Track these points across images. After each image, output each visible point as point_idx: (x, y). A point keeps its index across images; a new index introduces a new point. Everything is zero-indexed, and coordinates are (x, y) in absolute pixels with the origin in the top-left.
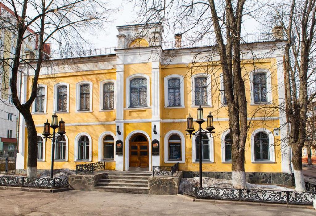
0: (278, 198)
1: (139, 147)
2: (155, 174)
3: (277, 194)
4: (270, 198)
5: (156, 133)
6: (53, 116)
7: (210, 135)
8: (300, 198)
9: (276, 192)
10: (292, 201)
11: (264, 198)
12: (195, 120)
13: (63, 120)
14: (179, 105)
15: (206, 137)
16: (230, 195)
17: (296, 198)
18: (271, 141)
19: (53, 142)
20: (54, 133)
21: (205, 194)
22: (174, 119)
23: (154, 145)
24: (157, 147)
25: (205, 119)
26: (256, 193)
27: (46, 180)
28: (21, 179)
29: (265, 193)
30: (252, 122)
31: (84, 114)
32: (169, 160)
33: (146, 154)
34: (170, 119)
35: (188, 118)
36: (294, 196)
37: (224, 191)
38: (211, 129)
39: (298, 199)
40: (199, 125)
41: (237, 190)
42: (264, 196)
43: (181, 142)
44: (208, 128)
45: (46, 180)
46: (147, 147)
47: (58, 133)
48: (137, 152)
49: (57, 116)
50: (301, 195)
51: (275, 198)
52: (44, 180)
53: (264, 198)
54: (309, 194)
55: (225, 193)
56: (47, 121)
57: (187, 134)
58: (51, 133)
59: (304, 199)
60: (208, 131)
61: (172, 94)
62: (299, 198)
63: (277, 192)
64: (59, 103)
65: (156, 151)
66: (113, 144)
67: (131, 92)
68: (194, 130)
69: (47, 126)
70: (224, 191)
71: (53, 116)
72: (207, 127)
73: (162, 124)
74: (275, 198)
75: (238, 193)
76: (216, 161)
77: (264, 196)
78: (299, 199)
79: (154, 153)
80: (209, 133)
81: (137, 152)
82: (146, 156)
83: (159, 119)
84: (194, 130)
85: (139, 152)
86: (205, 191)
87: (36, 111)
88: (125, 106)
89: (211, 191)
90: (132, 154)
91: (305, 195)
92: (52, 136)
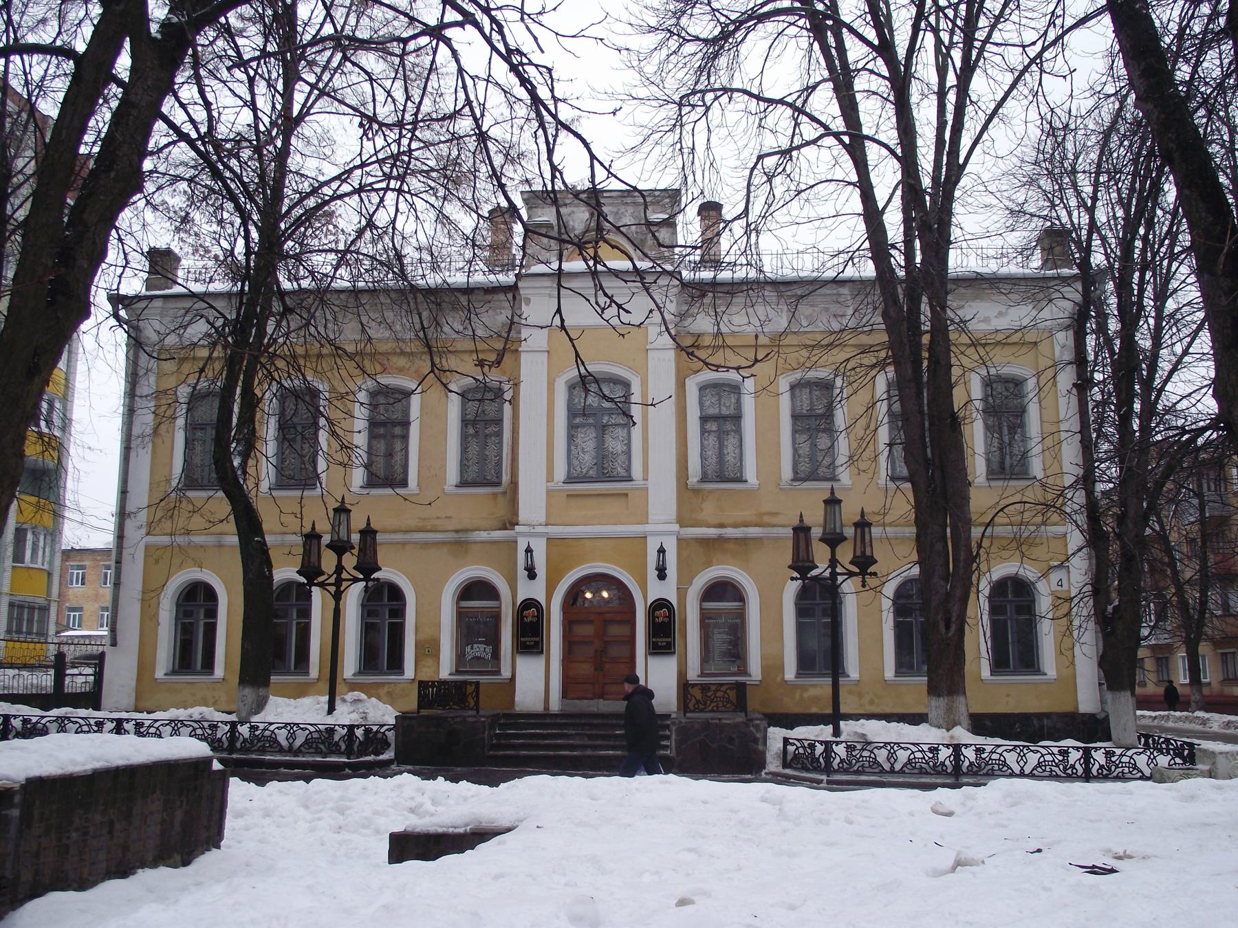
0: (1061, 767)
2: (691, 706)
3: (1058, 756)
4: (1039, 769)
5: (532, 575)
9: (925, 748)
11: (1022, 768)
12: (817, 532)
13: (374, 525)
14: (629, 479)
16: (1057, 766)
18: (1044, 604)
20: (340, 568)
21: (983, 765)
22: (722, 526)
25: (849, 532)
26: (872, 752)
27: (804, 747)
28: (820, 749)
29: (1024, 755)
30: (986, 543)
34: (709, 526)
35: (361, 532)
36: (1103, 762)
39: (1113, 768)
41: (947, 746)
42: (1022, 763)
43: (500, 608)
44: (829, 537)
45: (804, 747)
47: (851, 563)
51: (1053, 768)
52: (799, 745)
53: (1022, 768)
56: (369, 519)
58: (324, 568)
60: (857, 570)
61: (712, 441)
63: (929, 749)
64: (283, 454)
66: (496, 617)
67: (572, 428)
68: (322, 573)
69: (802, 535)
74: (1053, 768)
75: (1080, 760)
77: (1022, 763)
78: (1117, 767)
84: (322, 573)
87: (285, 480)
89: (1001, 755)
91: (1001, 755)
92: (332, 580)
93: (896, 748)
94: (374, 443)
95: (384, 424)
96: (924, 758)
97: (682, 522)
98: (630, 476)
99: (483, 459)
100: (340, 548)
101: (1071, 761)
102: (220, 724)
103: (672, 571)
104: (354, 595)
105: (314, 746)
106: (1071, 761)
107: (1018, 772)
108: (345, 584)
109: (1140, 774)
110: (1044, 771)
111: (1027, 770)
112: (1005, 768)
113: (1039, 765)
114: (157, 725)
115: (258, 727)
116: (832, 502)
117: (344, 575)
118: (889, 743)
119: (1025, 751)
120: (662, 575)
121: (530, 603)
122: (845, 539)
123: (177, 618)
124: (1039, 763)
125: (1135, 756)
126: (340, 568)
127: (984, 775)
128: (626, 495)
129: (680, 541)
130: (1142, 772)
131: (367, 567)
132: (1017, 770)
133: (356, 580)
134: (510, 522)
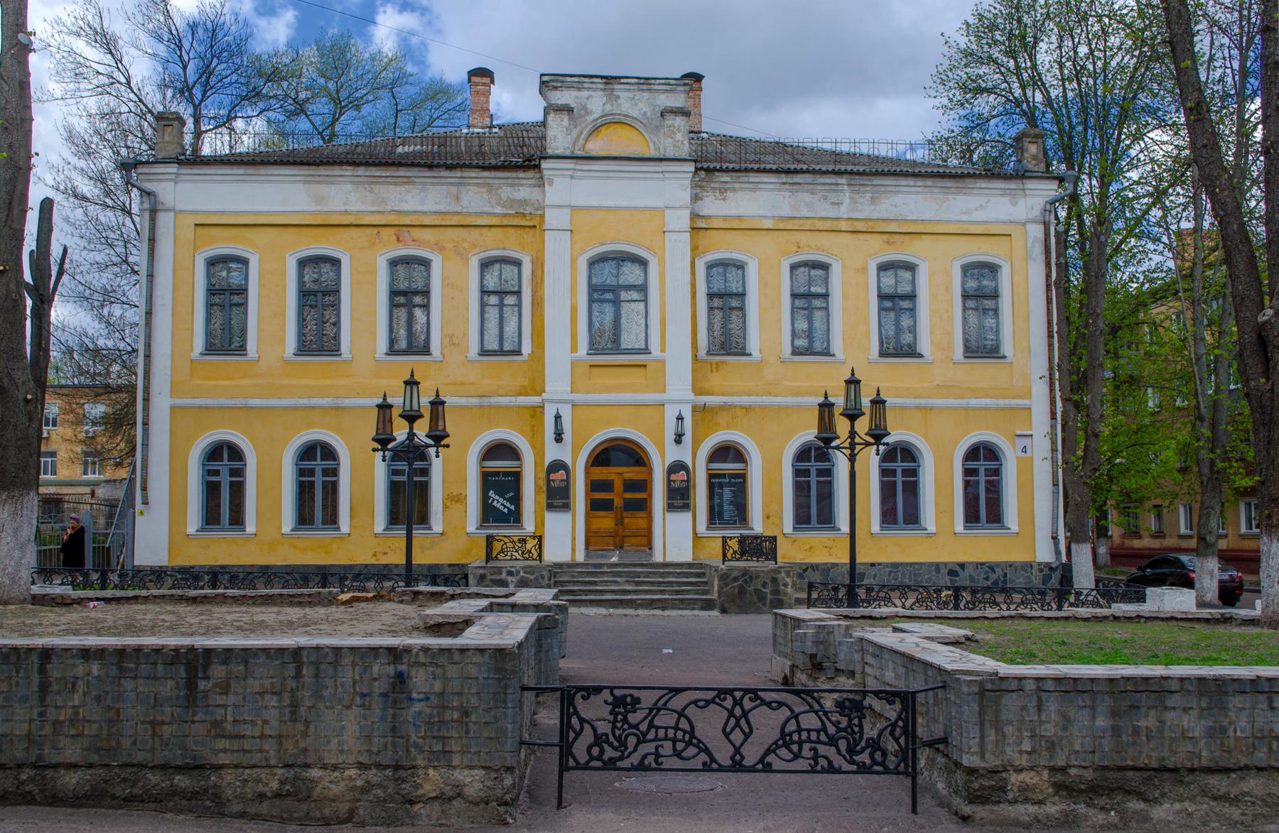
0: (843, 745)
1: (618, 485)
4: (783, 752)
6: (846, 381)
7: (437, 452)
8: (651, 735)
10: (592, 758)
11: (737, 750)
14: (646, 351)
15: (424, 457)
17: (618, 739)
19: (850, 460)
21: (632, 741)
23: (673, 477)
24: (563, 484)
29: (745, 714)
31: (984, 371)
32: (708, 528)
33: (643, 506)
37: (785, 713)
38: (438, 438)
39: (632, 741)
40: (406, 424)
42: (737, 737)
43: (520, 467)
44: (849, 412)
46: (644, 485)
48: (612, 501)
49: (858, 382)
50: (655, 710)
51: (822, 750)
53: (737, 750)
54: (708, 702)
55: (792, 726)
57: (374, 450)
59: (675, 741)
60: (432, 443)
62: (645, 734)
63: (839, 704)
65: (679, 498)
70: (785, 713)
71: (846, 381)
72: (377, 434)
73: (699, 410)
74: (822, 750)
76: (1164, 529)
78: (642, 740)
79: (556, 502)
80: (434, 449)
81: (612, 501)
82: (643, 514)
83: (689, 395)
85: (618, 502)
86: (633, 718)
88: (574, 348)
89: (681, 714)
90: (595, 506)
91: (681, 714)
93: (747, 704)
94: (395, 311)
95: (315, 293)
96: (824, 729)
97: (697, 391)
99: (227, 328)
100: (852, 416)
101: (870, 731)
102: (870, 700)
103: (567, 436)
104: (871, 461)
105: (806, 752)
106: (870, 731)
107: (728, 763)
108: (858, 447)
109: (703, 757)
110: (797, 756)
111: (751, 755)
112: (692, 751)
113: (785, 739)
114: (678, 702)
115: (636, 701)
116: (411, 383)
117: (857, 440)
118: (730, 692)
119: (747, 704)
120: (559, 438)
121: (557, 466)
122: (864, 414)
123: (203, 477)
124: (783, 734)
125: (691, 711)
126: (853, 434)
127: (633, 768)
129: (695, 409)
130: (707, 751)
131: (878, 435)
132: (723, 755)
133: (868, 444)
134: (536, 386)
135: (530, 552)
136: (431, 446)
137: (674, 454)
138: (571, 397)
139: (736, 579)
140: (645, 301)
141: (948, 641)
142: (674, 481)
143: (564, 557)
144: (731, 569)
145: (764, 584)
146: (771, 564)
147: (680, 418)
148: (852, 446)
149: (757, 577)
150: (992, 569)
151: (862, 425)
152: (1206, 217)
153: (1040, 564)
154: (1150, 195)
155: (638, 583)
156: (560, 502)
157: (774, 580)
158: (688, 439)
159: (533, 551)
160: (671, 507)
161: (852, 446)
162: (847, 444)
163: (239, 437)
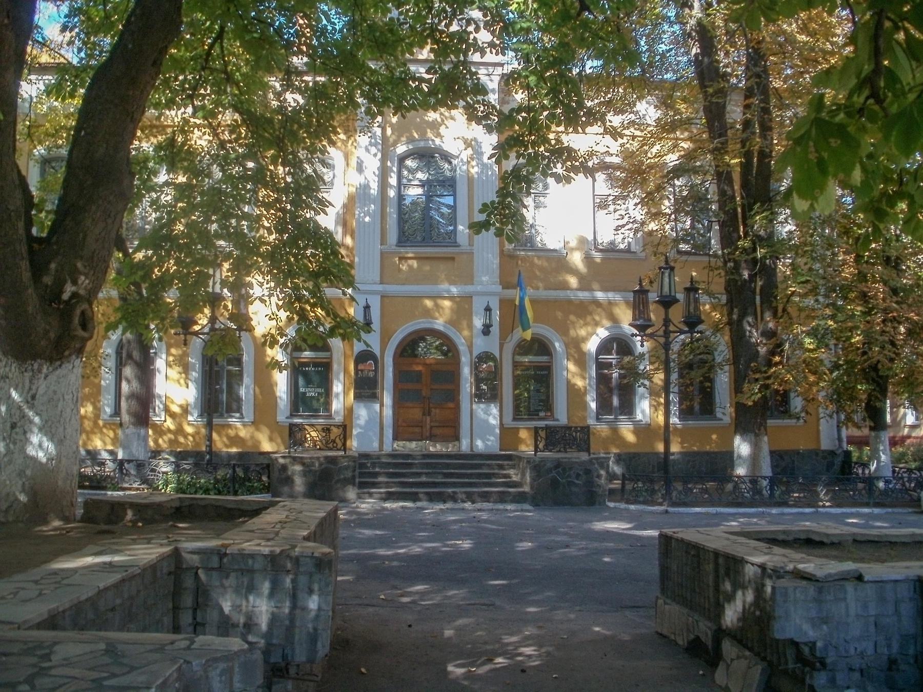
32: (514, 419)
33: (453, 395)
80: (639, 338)
98: (456, 242)
117: (672, 328)
122: (677, 301)
126: (667, 322)
128: (453, 259)
129: (504, 303)
135: (334, 441)
136: (636, 335)
137: (481, 345)
138: (380, 288)
139: (549, 471)
140: (454, 195)
141: (760, 536)
142: (362, 371)
143: (373, 446)
144: (543, 460)
145: (578, 476)
146: (584, 456)
147: (488, 309)
148: (667, 334)
149: (571, 469)
150: (781, 457)
151: (677, 314)
152: (308, 216)
153: (824, 451)
154: (421, 181)
155: (451, 475)
156: (368, 392)
157: (588, 472)
158: (495, 330)
159: (337, 440)
160: (479, 396)
161: (667, 334)
162: (661, 332)
163: (419, 323)
